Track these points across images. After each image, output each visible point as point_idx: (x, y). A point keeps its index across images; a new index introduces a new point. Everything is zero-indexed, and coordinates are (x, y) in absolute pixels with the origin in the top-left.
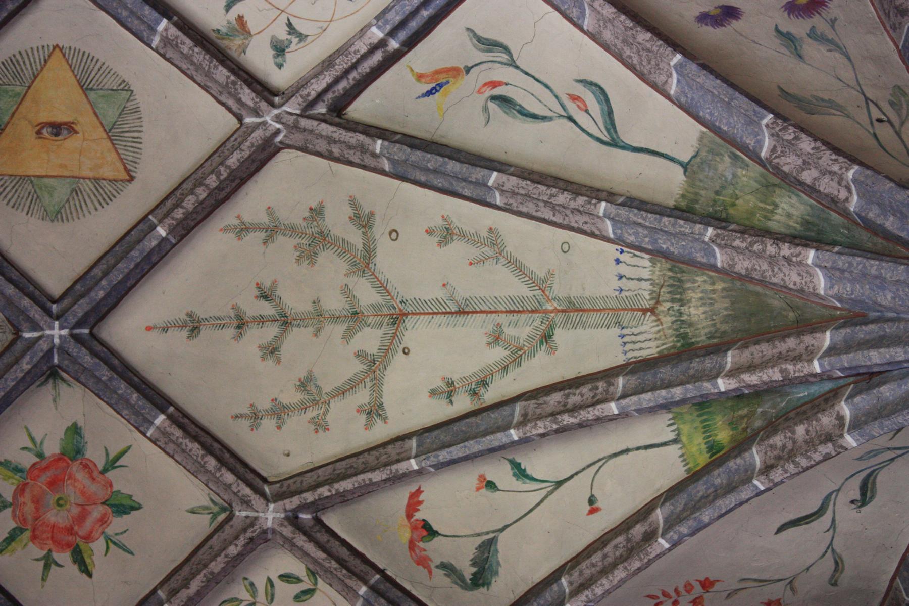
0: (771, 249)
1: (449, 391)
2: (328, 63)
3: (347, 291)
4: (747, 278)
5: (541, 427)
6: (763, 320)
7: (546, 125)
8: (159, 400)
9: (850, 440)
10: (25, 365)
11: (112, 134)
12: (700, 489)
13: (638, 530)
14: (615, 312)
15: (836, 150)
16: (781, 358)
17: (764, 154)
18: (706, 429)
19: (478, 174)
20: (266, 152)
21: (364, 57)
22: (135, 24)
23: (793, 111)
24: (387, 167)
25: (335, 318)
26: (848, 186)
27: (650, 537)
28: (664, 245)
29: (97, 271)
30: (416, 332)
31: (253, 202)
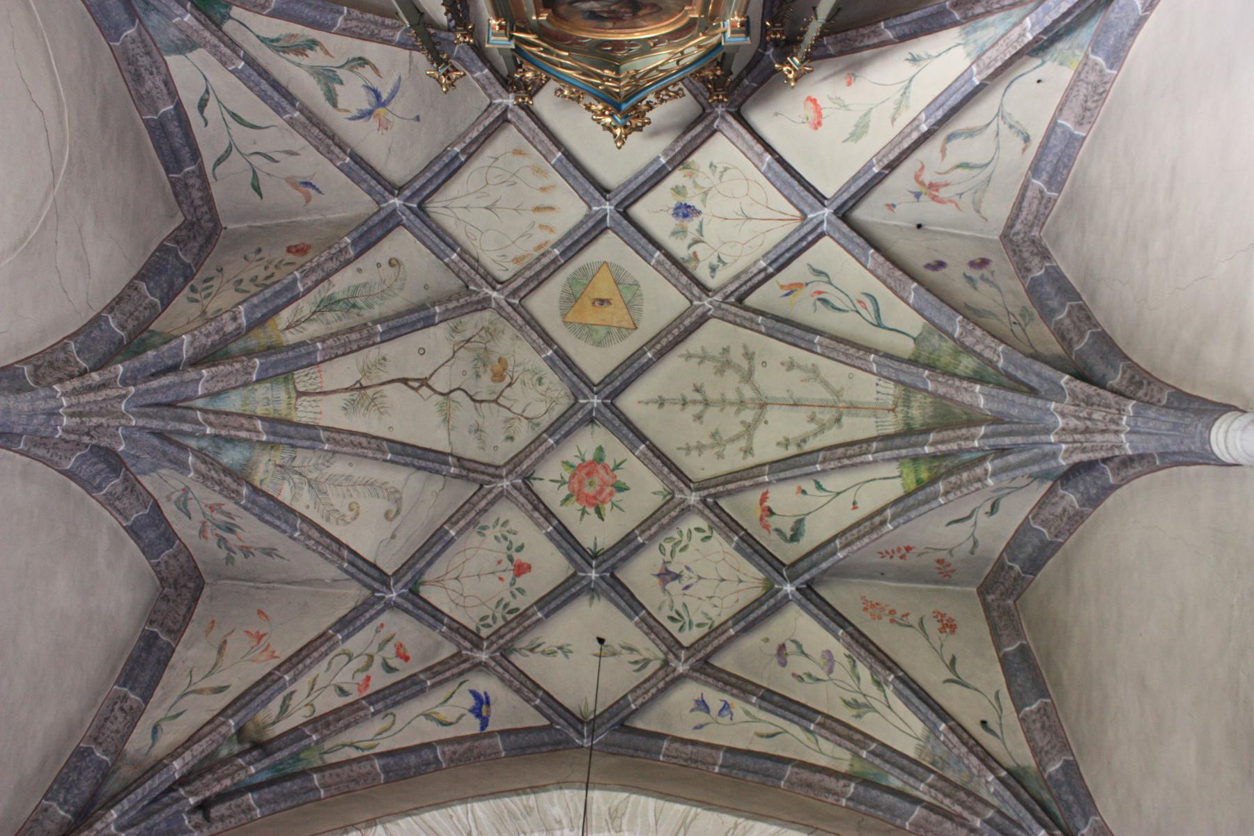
0: (957, 383)
1: (786, 443)
2: (737, 277)
3: (738, 390)
4: (944, 397)
5: (832, 464)
6: (950, 418)
7: (844, 315)
8: (643, 438)
9: (990, 482)
10: (580, 415)
11: (628, 306)
12: (911, 501)
13: (877, 520)
14: (874, 410)
15: (994, 336)
16: (959, 438)
17: (956, 335)
18: (916, 471)
19: (809, 336)
20: (703, 319)
21: (756, 275)
22: (643, 252)
23: (972, 315)
24: (763, 330)
25: (732, 404)
26: (999, 355)
27: (883, 523)
28: (902, 378)
29: (617, 373)
30: (772, 413)
31: (695, 343)
